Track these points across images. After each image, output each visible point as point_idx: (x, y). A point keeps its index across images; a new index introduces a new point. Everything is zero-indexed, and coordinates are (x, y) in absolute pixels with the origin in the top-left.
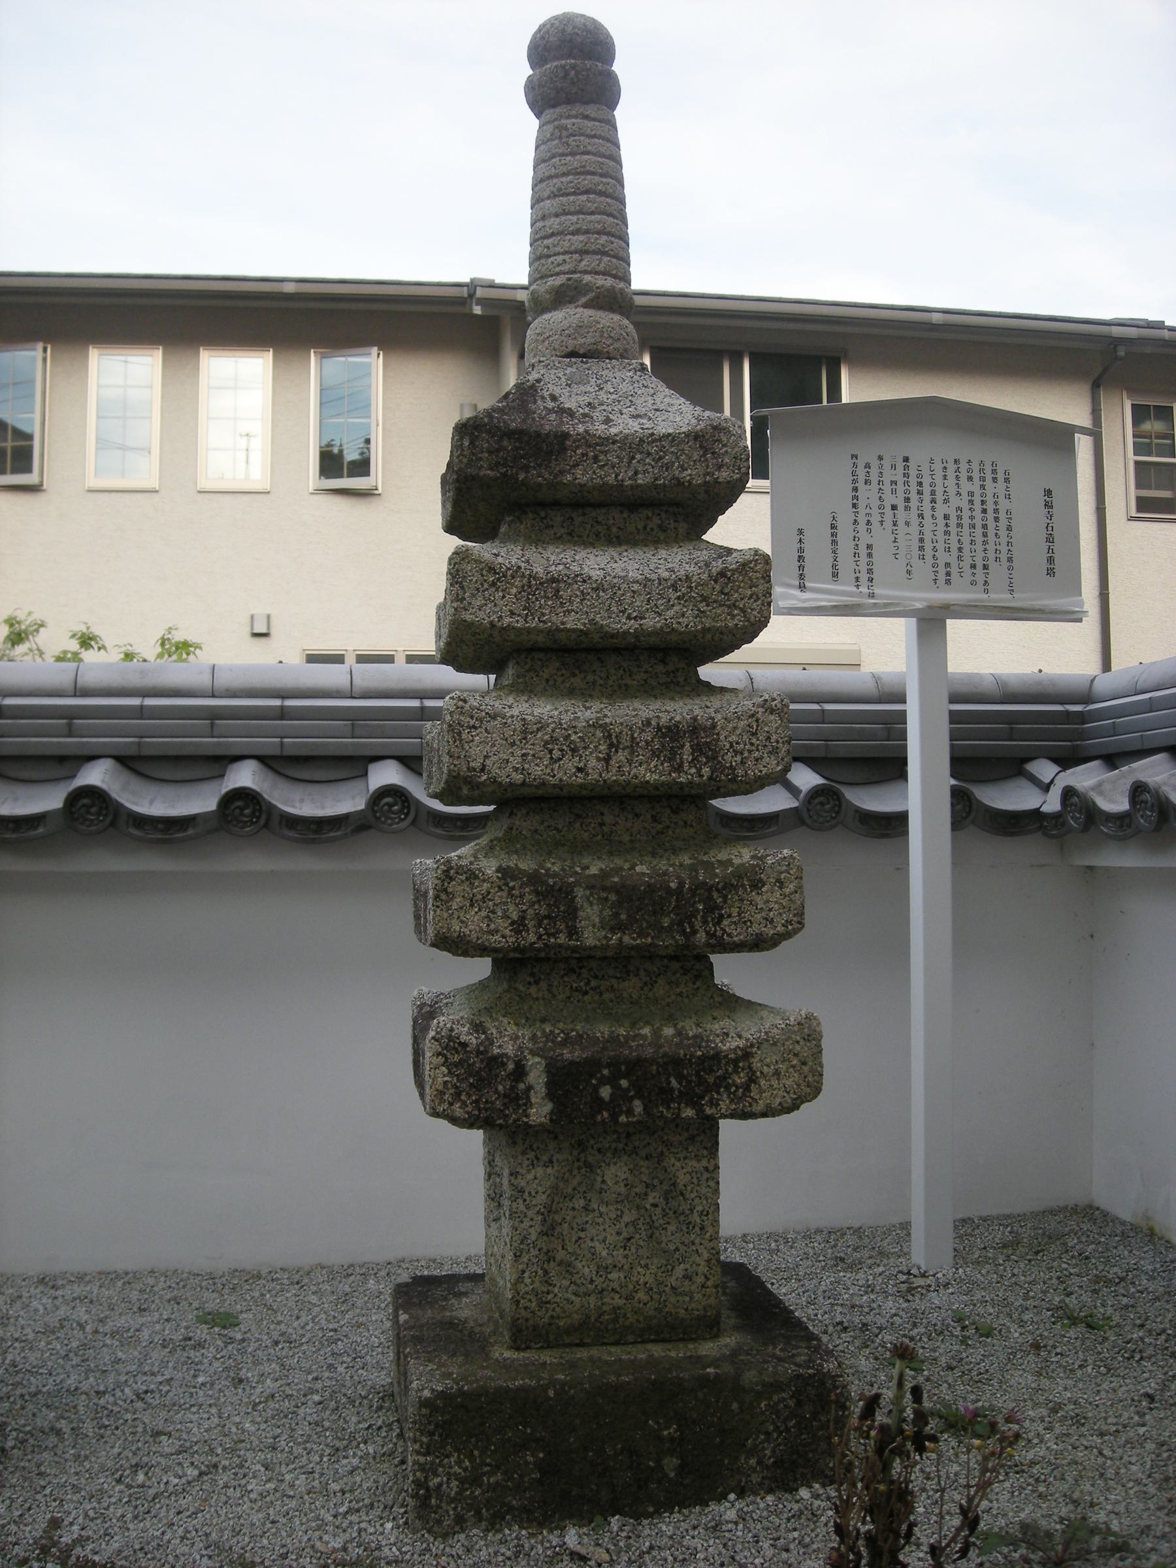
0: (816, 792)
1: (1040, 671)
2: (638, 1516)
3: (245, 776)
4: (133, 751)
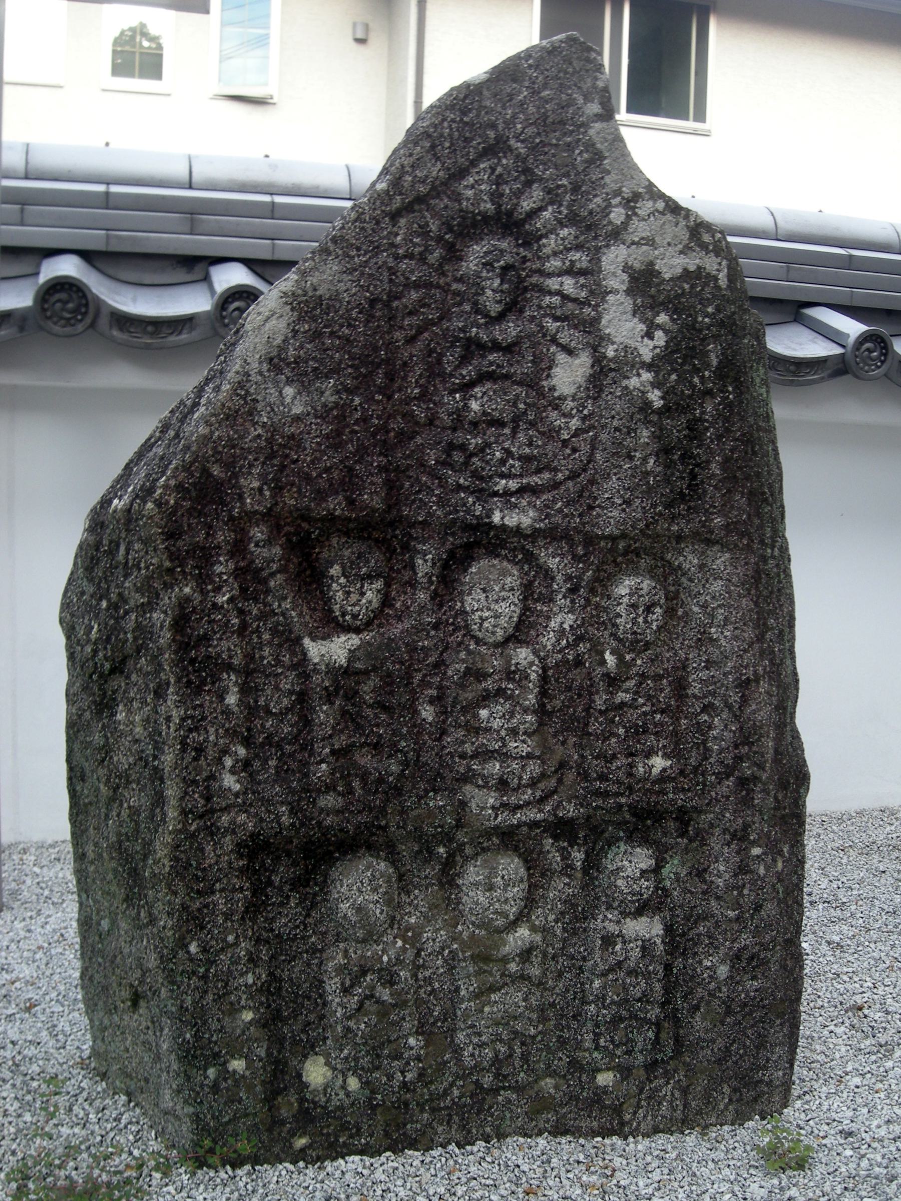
0: (864, 338)
2: (87, 1012)
3: (67, 267)
4: (100, 246)
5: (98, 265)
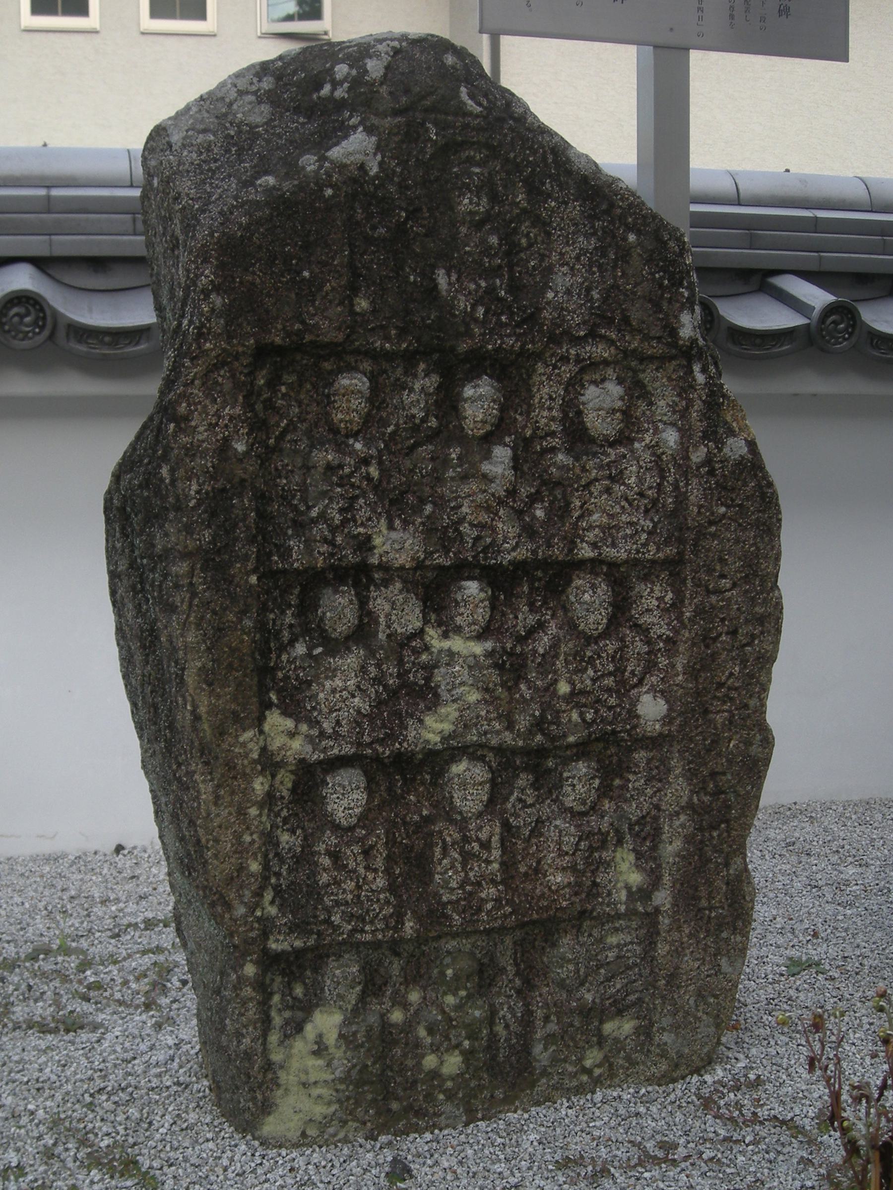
0: (830, 310)
1: (45, 145)
5: (50, 272)
